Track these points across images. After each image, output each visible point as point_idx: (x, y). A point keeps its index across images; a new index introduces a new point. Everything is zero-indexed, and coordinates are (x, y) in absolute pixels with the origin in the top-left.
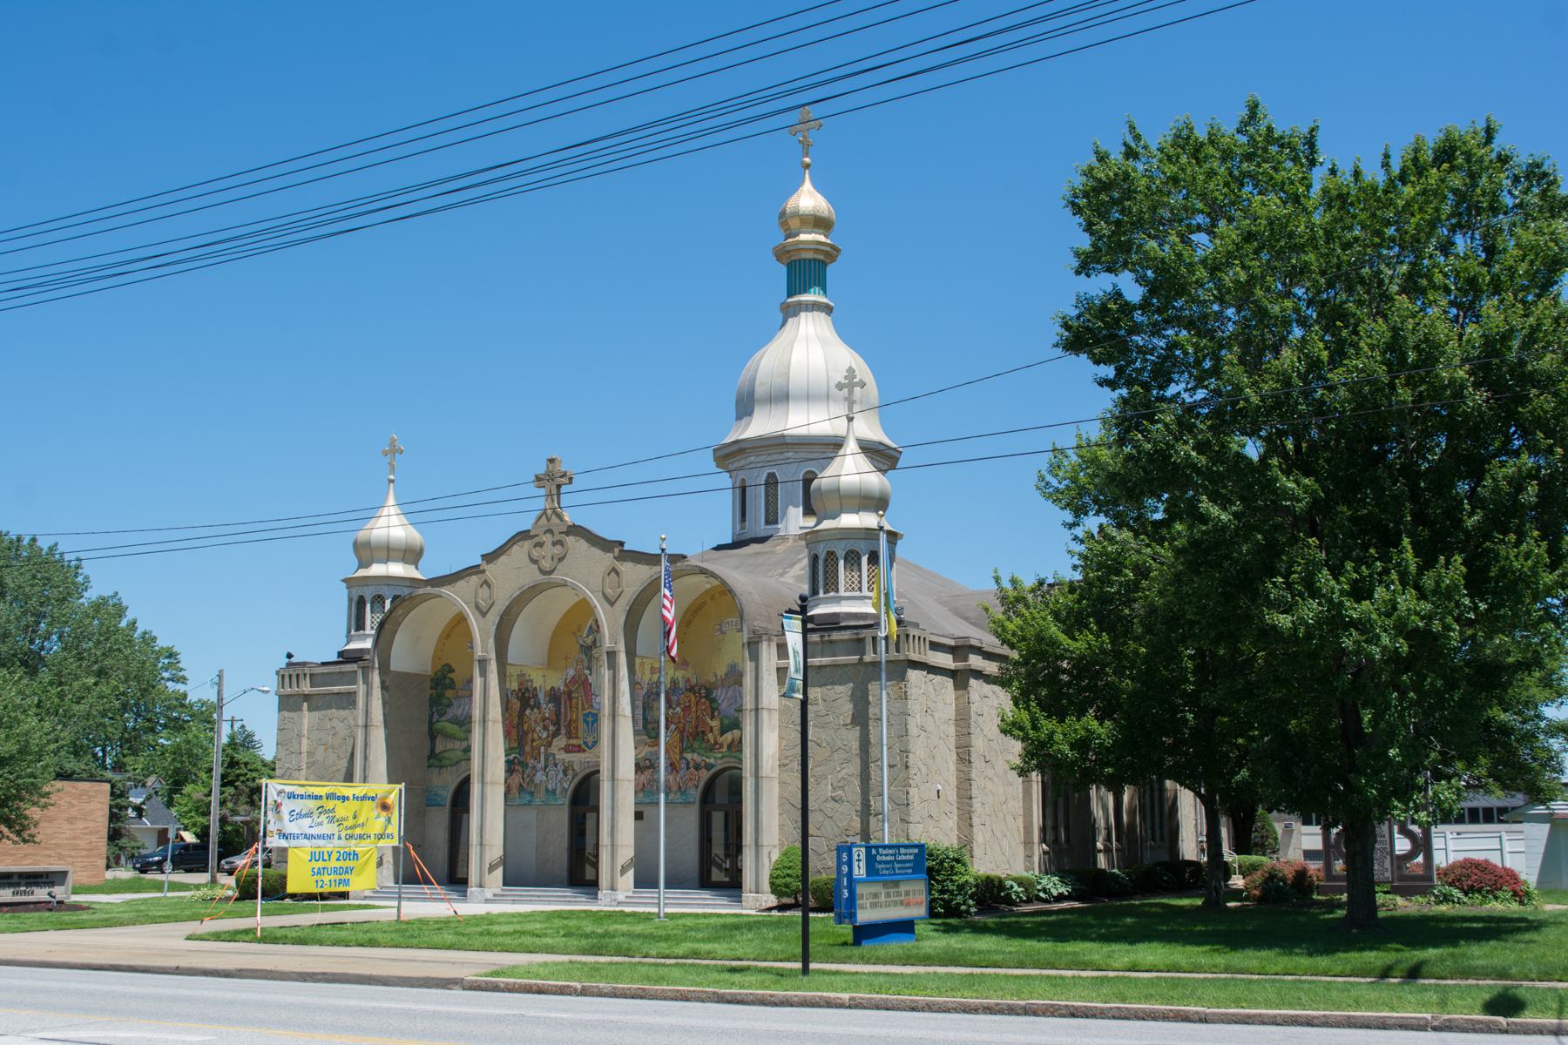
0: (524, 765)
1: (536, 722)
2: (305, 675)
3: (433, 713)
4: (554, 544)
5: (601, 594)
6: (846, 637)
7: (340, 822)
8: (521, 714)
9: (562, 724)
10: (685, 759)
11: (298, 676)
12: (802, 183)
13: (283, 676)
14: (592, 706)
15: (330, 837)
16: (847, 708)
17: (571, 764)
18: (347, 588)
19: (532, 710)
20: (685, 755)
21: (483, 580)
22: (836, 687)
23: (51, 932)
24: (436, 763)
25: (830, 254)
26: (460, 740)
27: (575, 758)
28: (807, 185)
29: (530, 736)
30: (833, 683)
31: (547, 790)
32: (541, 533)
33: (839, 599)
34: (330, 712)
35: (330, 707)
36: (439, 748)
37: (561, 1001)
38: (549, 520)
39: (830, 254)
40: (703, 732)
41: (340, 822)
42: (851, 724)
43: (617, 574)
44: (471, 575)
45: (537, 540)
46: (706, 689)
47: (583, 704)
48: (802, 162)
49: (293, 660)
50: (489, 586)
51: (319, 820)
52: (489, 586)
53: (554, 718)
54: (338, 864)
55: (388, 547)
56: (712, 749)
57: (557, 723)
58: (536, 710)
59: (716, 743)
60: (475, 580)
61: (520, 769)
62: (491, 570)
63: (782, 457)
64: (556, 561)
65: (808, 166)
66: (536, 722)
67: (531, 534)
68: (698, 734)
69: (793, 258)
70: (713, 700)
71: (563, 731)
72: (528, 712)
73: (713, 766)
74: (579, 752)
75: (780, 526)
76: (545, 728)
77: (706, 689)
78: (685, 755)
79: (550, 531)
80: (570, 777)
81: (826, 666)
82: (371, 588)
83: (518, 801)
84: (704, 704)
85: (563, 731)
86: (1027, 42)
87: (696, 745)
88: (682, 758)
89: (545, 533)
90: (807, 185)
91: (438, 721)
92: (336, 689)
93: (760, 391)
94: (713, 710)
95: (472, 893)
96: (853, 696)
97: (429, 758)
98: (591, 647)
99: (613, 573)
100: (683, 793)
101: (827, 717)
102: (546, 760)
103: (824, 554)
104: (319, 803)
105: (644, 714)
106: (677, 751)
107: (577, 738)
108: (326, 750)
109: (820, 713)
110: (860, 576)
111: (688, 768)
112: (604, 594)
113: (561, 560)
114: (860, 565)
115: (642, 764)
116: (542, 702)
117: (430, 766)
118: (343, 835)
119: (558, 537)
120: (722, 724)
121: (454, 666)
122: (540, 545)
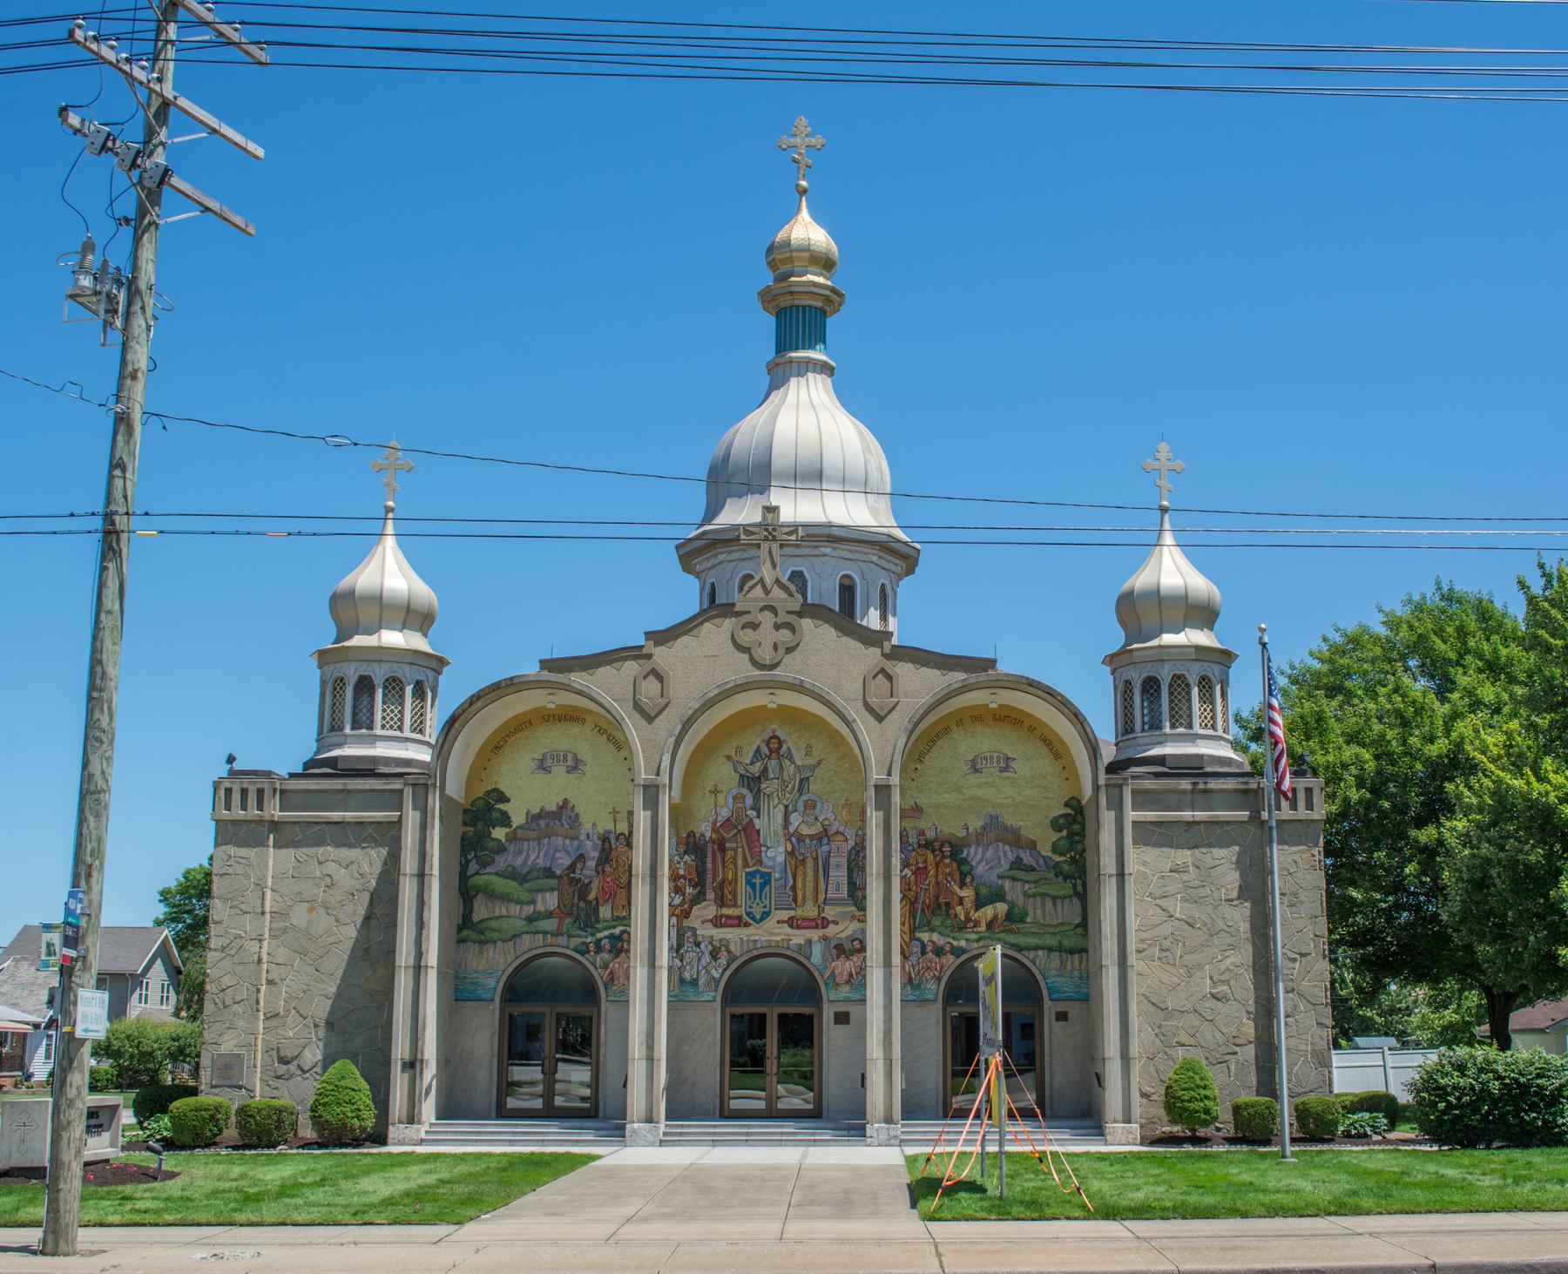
2: (275, 790)
3: (468, 862)
4: (777, 627)
5: (860, 704)
6: (1230, 786)
9: (708, 884)
10: (918, 939)
11: (260, 792)
12: (799, 209)
13: (229, 791)
14: (760, 862)
16: (1231, 879)
17: (725, 944)
18: (320, 667)
20: (918, 935)
21: (648, 668)
22: (1213, 850)
23: (1173, 1222)
24: (474, 936)
25: (832, 300)
26: (520, 902)
27: (732, 934)
28: (804, 214)
30: (1210, 845)
33: (1195, 738)
34: (321, 850)
35: (320, 842)
36: (480, 911)
38: (767, 592)
39: (832, 300)
40: (947, 904)
42: (1238, 898)
43: (889, 678)
44: (625, 659)
45: (746, 618)
46: (951, 845)
47: (745, 858)
48: (798, 185)
49: (237, 766)
50: (660, 678)
52: (660, 678)
53: (694, 875)
55: (408, 607)
56: (962, 927)
57: (700, 884)
59: (968, 919)
60: (631, 667)
62: (663, 656)
63: (816, 552)
64: (781, 651)
65: (805, 191)
67: (737, 609)
68: (939, 907)
69: (796, 302)
70: (965, 861)
71: (710, 895)
73: (964, 951)
74: (739, 926)
77: (951, 845)
78: (918, 935)
79: (773, 610)
80: (723, 961)
81: (1199, 823)
82: (386, 666)
84: (948, 866)
85: (710, 895)
87: (936, 922)
90: (804, 214)
91: (477, 873)
92: (336, 815)
93: (778, 463)
94: (963, 875)
95: (634, 1131)
96: (1239, 863)
97: (460, 928)
98: (759, 777)
101: (1202, 890)
103: (356, 677)
105: (850, 877)
107: (735, 906)
108: (311, 909)
109: (1191, 884)
110: (401, 712)
111: (923, 953)
113: (789, 650)
114: (402, 697)
115: (847, 946)
117: (461, 941)
119: (782, 618)
120: (977, 894)
121: (508, 793)
122: (754, 626)
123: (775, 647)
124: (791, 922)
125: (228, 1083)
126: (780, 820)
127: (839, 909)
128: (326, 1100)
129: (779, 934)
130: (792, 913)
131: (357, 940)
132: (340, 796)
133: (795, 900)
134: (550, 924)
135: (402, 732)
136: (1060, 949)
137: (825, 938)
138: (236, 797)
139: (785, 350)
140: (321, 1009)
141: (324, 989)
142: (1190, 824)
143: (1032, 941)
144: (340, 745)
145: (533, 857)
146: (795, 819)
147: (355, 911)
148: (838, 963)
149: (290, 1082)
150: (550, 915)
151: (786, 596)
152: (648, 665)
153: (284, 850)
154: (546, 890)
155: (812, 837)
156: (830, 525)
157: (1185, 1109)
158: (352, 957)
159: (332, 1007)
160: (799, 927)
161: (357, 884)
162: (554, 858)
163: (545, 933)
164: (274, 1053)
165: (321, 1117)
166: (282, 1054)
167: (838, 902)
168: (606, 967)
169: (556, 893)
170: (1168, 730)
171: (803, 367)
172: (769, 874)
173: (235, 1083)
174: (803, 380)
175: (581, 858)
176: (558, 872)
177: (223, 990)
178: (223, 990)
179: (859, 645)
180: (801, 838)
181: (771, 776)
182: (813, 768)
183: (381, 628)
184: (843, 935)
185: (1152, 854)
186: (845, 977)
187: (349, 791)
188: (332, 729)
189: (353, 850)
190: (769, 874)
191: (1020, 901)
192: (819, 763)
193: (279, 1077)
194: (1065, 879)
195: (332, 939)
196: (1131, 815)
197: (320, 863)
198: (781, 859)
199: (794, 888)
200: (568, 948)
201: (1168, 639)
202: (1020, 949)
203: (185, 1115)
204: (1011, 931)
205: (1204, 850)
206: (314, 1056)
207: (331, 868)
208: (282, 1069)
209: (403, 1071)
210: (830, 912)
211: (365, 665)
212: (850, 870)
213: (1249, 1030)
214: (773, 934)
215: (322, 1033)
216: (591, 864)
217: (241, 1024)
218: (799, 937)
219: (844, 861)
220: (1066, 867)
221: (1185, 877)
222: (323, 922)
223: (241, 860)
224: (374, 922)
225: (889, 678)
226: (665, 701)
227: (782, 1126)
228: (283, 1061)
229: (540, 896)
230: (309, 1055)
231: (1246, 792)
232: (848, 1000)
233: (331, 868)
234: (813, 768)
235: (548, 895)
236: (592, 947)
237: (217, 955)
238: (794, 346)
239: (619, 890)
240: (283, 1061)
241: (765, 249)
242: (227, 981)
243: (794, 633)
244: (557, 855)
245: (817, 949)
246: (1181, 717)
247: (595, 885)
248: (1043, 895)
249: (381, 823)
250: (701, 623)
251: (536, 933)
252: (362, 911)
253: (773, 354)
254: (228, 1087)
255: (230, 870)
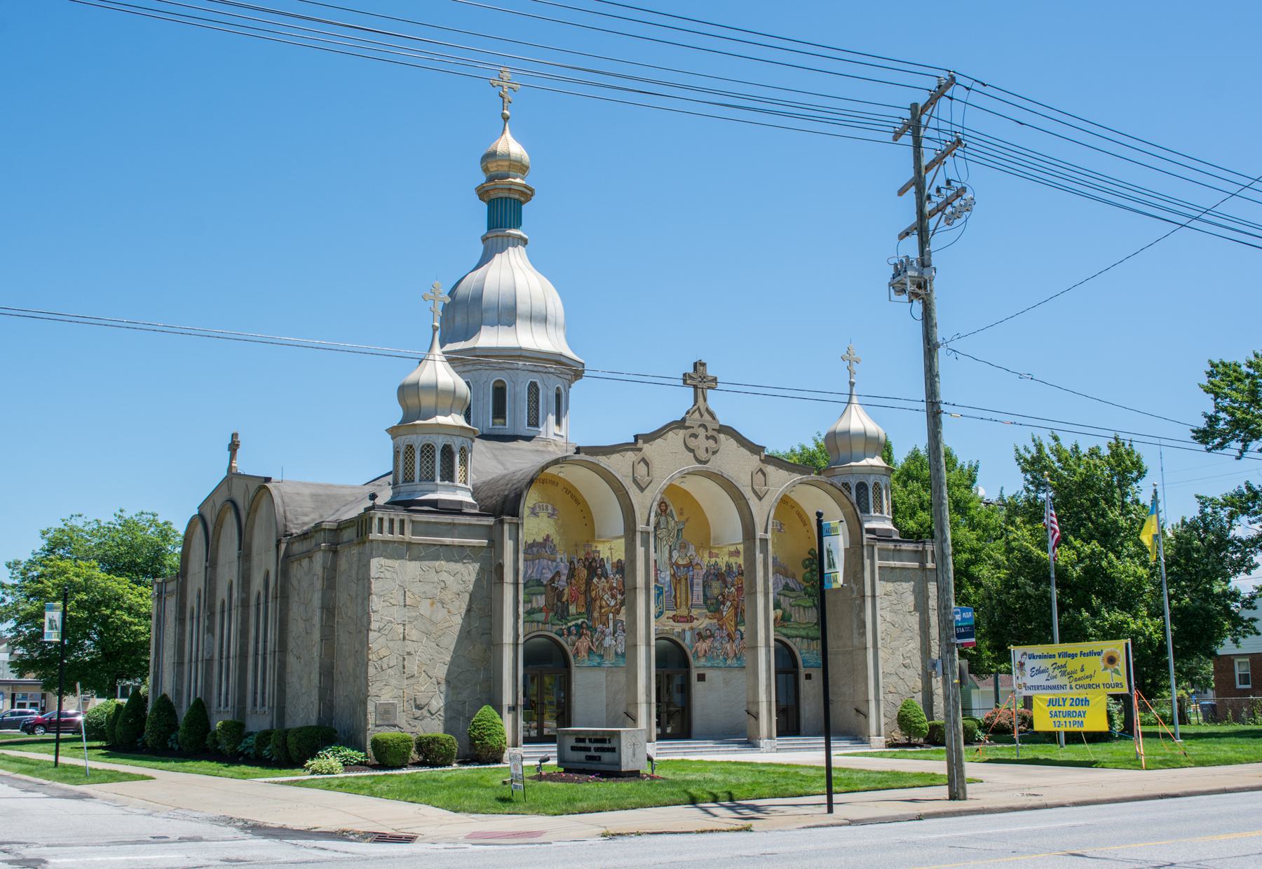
0: (593, 629)
1: (603, 590)
4: (707, 438)
5: (750, 488)
6: (910, 548)
7: (1070, 675)
8: (589, 583)
10: (739, 631)
15: (1063, 687)
16: (910, 599)
19: (600, 578)
20: (739, 627)
22: (903, 583)
29: (598, 602)
30: (901, 581)
31: (616, 653)
32: (696, 427)
34: (437, 563)
35: (437, 558)
37: (1171, 803)
38: (702, 415)
39: (527, 194)
41: (1070, 675)
43: (764, 474)
44: (627, 450)
48: (503, 114)
50: (647, 464)
51: (1054, 674)
52: (647, 464)
54: (1072, 709)
58: (603, 579)
60: (630, 456)
61: (589, 633)
62: (648, 449)
64: (710, 453)
66: (603, 590)
72: (595, 580)
75: (541, 429)
76: (613, 597)
78: (739, 627)
79: (704, 426)
82: (421, 437)
83: (587, 663)
86: (1031, 177)
88: (737, 630)
89: (699, 426)
92: (448, 540)
99: (760, 473)
100: (738, 659)
102: (615, 626)
104: (1053, 661)
105: (704, 591)
106: (733, 623)
108: (432, 604)
112: (753, 489)
113: (714, 453)
115: (704, 634)
116: (609, 572)
118: (1074, 684)
119: (710, 433)
122: (695, 436)
123: (707, 450)
124: (675, 618)
125: (387, 723)
126: (667, 555)
127: (699, 611)
128: (489, 732)
129: (668, 626)
130: (674, 613)
131: (462, 626)
132: (448, 527)
133: (676, 605)
134: (540, 616)
135: (403, 482)
136: (807, 637)
137: (692, 629)
138: (386, 524)
139: (505, 227)
140: (441, 672)
141: (441, 659)
142: (893, 568)
143: (794, 632)
144: (433, 491)
145: (529, 572)
146: (675, 554)
147: (460, 605)
148: (699, 644)
149: (423, 722)
150: (541, 610)
151: (711, 419)
152: (640, 455)
153: (414, 562)
154: (538, 594)
155: (684, 566)
156: (520, 349)
157: (917, 728)
158: (460, 637)
159: (448, 670)
160: (678, 622)
161: (461, 588)
162: (542, 573)
163: (538, 622)
164: (412, 702)
165: (487, 743)
166: (418, 702)
167: (698, 606)
168: (574, 645)
169: (544, 596)
170: (872, 514)
171: (516, 242)
172: (662, 588)
173: (392, 723)
174: (516, 249)
175: (558, 573)
176: (545, 583)
177: (381, 659)
178: (381, 659)
179: (748, 453)
180: (678, 566)
181: (662, 527)
182: (684, 523)
183: (451, 412)
184: (701, 627)
185: (890, 586)
186: (703, 652)
187: (454, 524)
188: (405, 481)
189: (458, 564)
190: (662, 588)
191: (788, 608)
192: (687, 520)
193: (416, 719)
194: (809, 597)
195: (447, 624)
196: (878, 563)
197: (437, 572)
198: (668, 579)
199: (675, 596)
200: (552, 632)
201: (441, 419)
202: (789, 637)
203: (399, 745)
204: (784, 626)
205: (898, 583)
206: (438, 703)
207: (444, 576)
208: (418, 713)
209: (509, 713)
210: (694, 612)
211: (448, 437)
212: (704, 587)
213: (919, 684)
214: (664, 625)
215: (443, 687)
216: (564, 578)
217: (393, 682)
218: (678, 627)
219: (701, 581)
220: (809, 589)
221: (891, 598)
222: (441, 614)
223: (389, 569)
224: (472, 614)
225: (764, 474)
226: (649, 479)
227: (706, 743)
228: (419, 707)
229: (534, 597)
230: (435, 703)
231: (916, 552)
232: (704, 667)
233: (444, 576)
234: (684, 523)
235: (539, 597)
236: (565, 631)
237: (376, 634)
238: (508, 225)
239: (580, 596)
240: (419, 707)
241: (481, 156)
242: (383, 652)
243: (716, 442)
244: (544, 571)
245: (688, 635)
246: (448, 475)
247: (566, 591)
248: (799, 606)
249: (474, 547)
250: (668, 432)
251: (533, 622)
252: (464, 607)
253: (486, 230)
254: (387, 726)
255: (382, 575)
